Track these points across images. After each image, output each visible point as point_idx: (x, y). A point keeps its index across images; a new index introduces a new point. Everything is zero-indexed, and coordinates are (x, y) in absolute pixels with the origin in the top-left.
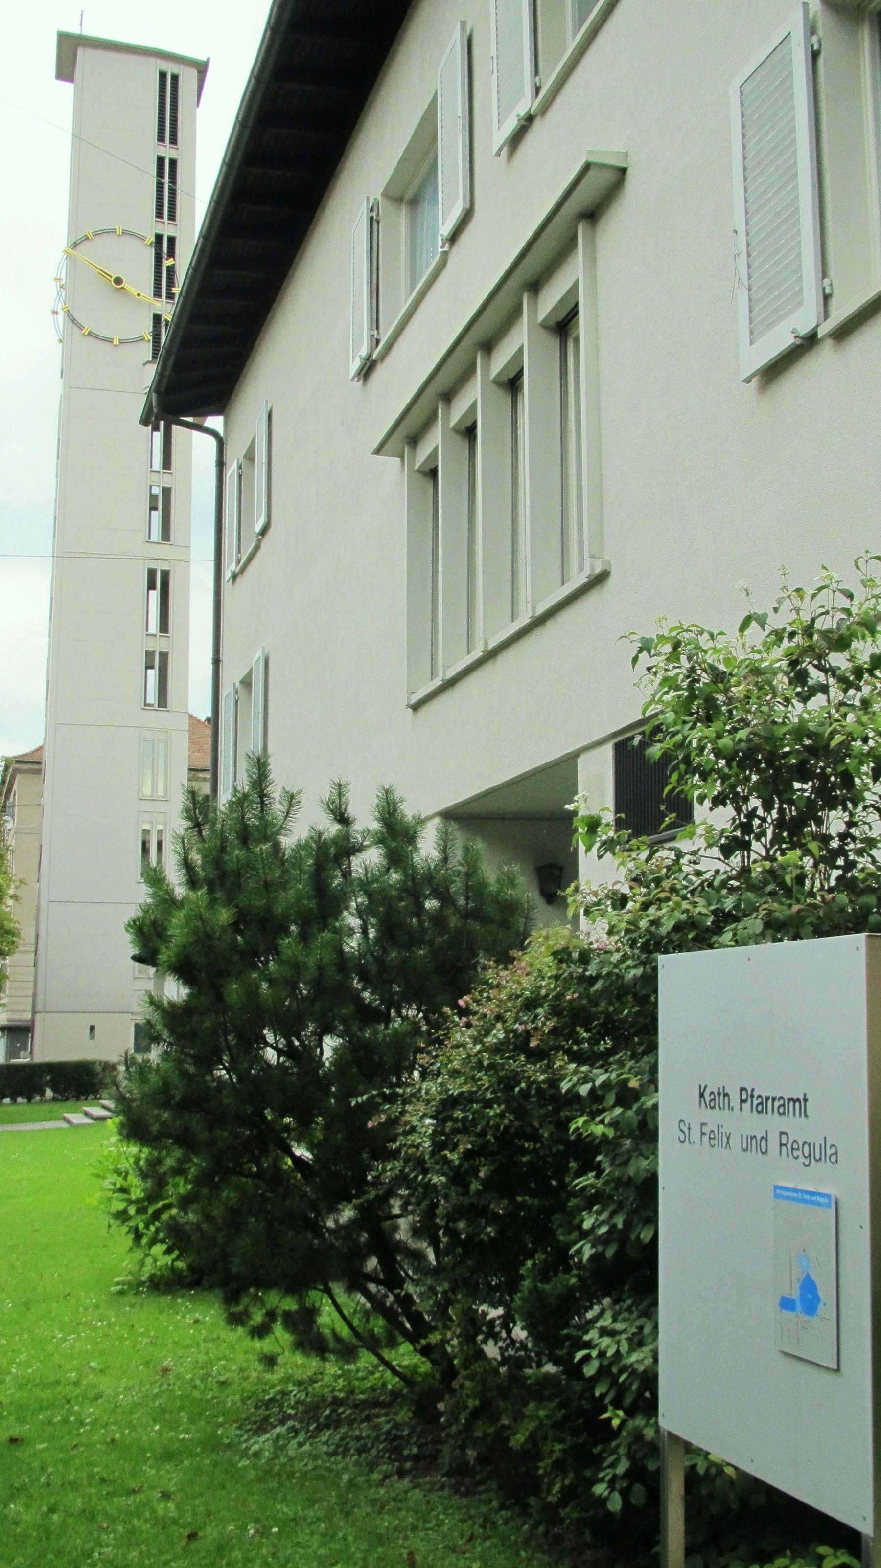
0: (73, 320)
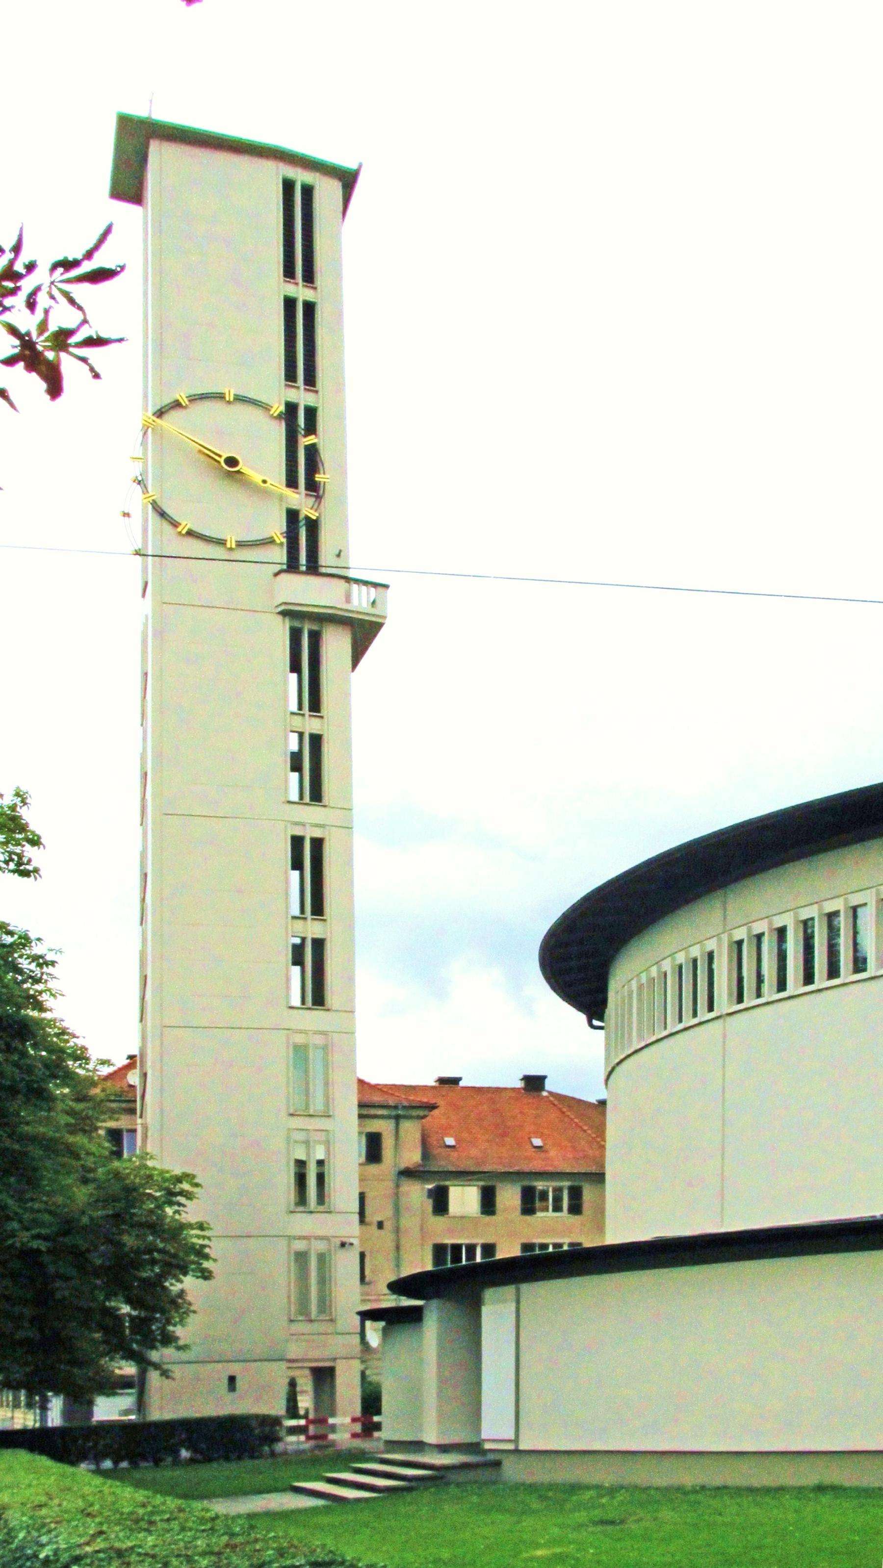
0: (162, 514)
